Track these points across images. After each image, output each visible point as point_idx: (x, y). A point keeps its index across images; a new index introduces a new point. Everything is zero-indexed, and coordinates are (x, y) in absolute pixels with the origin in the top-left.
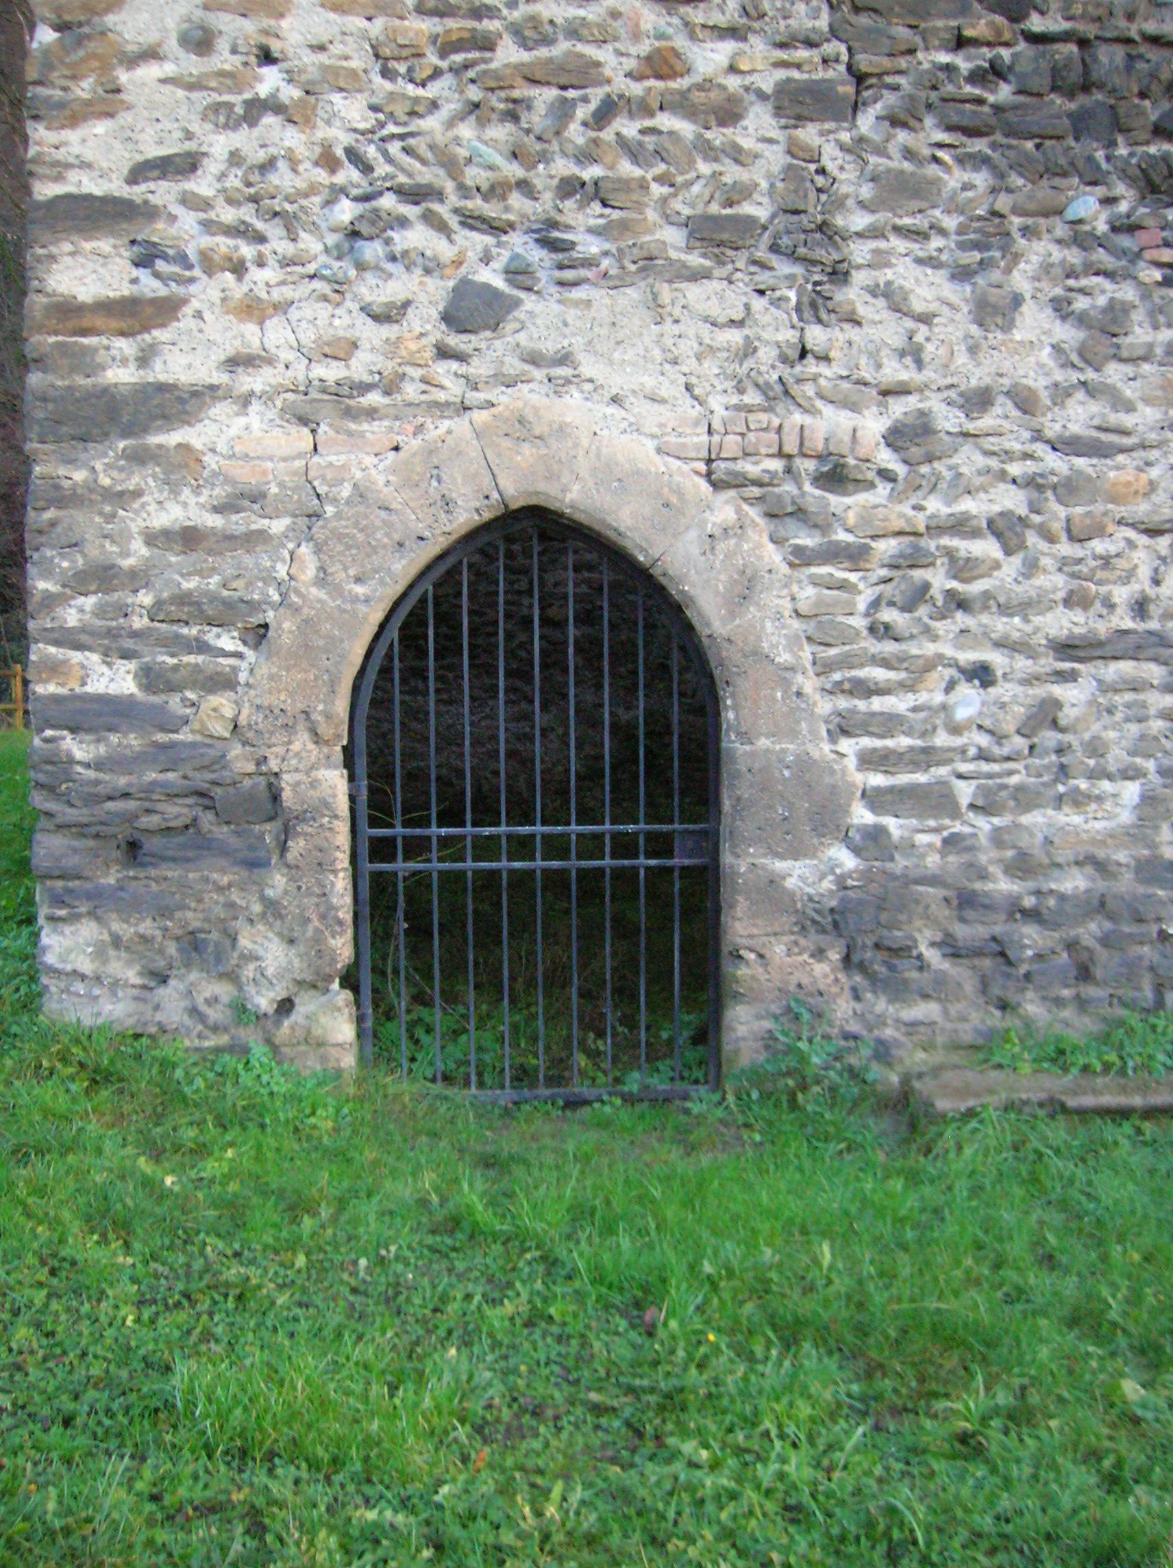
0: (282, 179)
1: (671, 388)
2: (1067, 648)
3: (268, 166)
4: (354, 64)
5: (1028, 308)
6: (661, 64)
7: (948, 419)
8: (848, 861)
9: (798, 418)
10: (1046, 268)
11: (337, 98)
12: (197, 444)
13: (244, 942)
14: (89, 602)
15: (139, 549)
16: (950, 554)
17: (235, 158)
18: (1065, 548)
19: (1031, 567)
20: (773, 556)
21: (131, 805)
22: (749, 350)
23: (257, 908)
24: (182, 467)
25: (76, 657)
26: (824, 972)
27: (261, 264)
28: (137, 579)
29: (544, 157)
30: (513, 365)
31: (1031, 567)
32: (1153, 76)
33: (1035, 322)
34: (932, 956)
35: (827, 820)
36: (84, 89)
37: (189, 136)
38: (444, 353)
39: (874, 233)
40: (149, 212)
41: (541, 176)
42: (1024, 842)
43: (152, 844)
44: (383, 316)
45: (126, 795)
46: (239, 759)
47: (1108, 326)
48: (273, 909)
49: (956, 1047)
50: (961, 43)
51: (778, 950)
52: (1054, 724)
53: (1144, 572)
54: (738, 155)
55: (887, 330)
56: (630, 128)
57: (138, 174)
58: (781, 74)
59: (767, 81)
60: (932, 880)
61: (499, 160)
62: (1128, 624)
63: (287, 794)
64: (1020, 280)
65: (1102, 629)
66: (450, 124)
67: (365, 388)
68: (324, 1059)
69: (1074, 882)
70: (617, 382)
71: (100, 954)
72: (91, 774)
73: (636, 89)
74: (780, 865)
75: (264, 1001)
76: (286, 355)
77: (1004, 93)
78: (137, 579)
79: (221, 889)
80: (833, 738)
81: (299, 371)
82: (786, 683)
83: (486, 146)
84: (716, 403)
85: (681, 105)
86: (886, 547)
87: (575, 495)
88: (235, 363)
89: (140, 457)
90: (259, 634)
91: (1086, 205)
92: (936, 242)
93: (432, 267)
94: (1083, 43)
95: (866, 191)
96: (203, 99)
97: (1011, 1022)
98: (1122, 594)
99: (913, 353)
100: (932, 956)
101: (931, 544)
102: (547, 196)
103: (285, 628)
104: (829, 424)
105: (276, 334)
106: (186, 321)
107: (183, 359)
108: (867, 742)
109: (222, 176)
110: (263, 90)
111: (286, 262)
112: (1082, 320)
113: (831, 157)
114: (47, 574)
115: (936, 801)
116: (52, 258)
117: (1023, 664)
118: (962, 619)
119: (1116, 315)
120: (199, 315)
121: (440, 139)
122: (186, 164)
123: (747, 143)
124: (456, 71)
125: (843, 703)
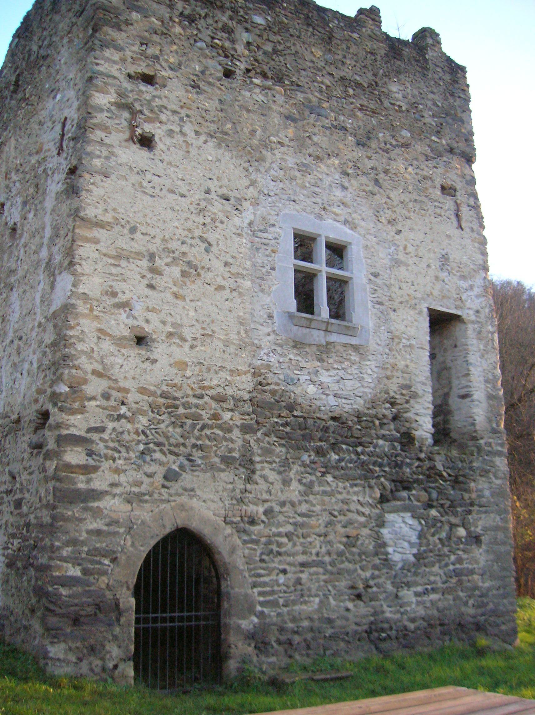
0: (126, 437)
1: (216, 499)
2: (303, 565)
3: (122, 433)
4: (145, 408)
5: (293, 481)
6: (216, 417)
7: (277, 508)
8: (256, 620)
9: (244, 507)
10: (297, 472)
11: (140, 417)
12: (102, 506)
13: (107, 648)
14: (70, 549)
15: (84, 535)
16: (277, 542)
17: (114, 429)
18: (302, 540)
19: (295, 545)
20: (239, 542)
21: (78, 608)
22: (234, 490)
23: (111, 638)
24: (97, 513)
25: (65, 564)
26: (250, 650)
27: (119, 459)
28: (83, 543)
29: (188, 438)
30: (180, 491)
31: (295, 545)
32: (319, 427)
33: (295, 485)
34: (274, 644)
35: (251, 610)
36: (76, 405)
37: (103, 422)
38: (164, 486)
39: (262, 462)
40: (91, 441)
41: (188, 442)
42: (294, 613)
43: (82, 619)
44: (150, 476)
45: (77, 605)
46: (109, 595)
47: (310, 486)
48: (115, 638)
49: (280, 668)
50: (279, 416)
51: (240, 644)
52: (300, 584)
53: (318, 546)
54: (232, 441)
55: (263, 486)
56: (208, 432)
57: (89, 430)
58: (242, 421)
59: (239, 423)
60: (274, 624)
61: (179, 438)
62: (315, 558)
63: (121, 605)
64: (292, 475)
65: (310, 560)
66: (167, 427)
67: (145, 494)
68: (127, 682)
69: (306, 624)
70: (205, 497)
71: (66, 653)
72: (67, 599)
73: (210, 422)
74: (241, 622)
75: (111, 665)
76: (125, 484)
77: (288, 429)
78: (83, 543)
79: (101, 632)
80: (252, 588)
81: (128, 488)
82: (242, 574)
83: (175, 433)
84: (226, 503)
85: (220, 427)
86: (263, 540)
87: (194, 525)
88: (112, 485)
89: (86, 509)
90: (114, 560)
91: (305, 458)
92: (274, 465)
93: (161, 464)
94: (304, 418)
95: (259, 452)
96: (107, 412)
97: (292, 660)
98: (314, 551)
99: (269, 492)
100: (274, 644)
101: (273, 539)
102: (189, 448)
103: (123, 558)
104: (252, 509)
105: (123, 478)
106: (100, 473)
107: (99, 482)
108: (260, 589)
109: (111, 434)
110: (122, 412)
111: (125, 459)
112: (305, 485)
113: (252, 443)
114: (59, 540)
115: (274, 604)
116: (65, 451)
117: (293, 569)
118: (280, 558)
119: (311, 484)
120: (103, 471)
121: (165, 430)
122: (101, 430)
123: (234, 438)
124: (169, 413)
125: (254, 579)
